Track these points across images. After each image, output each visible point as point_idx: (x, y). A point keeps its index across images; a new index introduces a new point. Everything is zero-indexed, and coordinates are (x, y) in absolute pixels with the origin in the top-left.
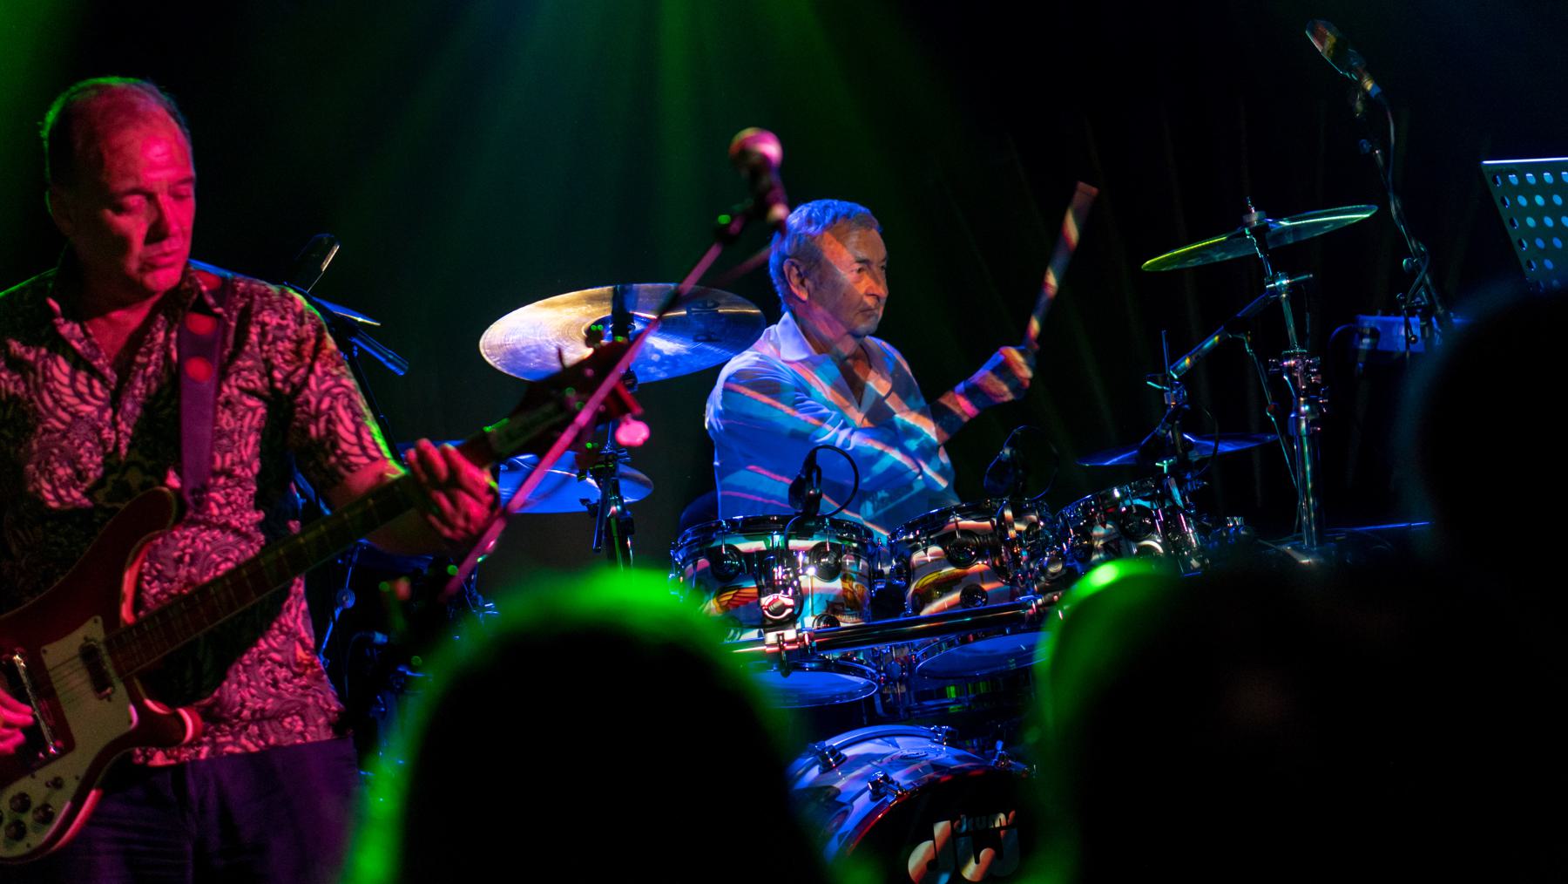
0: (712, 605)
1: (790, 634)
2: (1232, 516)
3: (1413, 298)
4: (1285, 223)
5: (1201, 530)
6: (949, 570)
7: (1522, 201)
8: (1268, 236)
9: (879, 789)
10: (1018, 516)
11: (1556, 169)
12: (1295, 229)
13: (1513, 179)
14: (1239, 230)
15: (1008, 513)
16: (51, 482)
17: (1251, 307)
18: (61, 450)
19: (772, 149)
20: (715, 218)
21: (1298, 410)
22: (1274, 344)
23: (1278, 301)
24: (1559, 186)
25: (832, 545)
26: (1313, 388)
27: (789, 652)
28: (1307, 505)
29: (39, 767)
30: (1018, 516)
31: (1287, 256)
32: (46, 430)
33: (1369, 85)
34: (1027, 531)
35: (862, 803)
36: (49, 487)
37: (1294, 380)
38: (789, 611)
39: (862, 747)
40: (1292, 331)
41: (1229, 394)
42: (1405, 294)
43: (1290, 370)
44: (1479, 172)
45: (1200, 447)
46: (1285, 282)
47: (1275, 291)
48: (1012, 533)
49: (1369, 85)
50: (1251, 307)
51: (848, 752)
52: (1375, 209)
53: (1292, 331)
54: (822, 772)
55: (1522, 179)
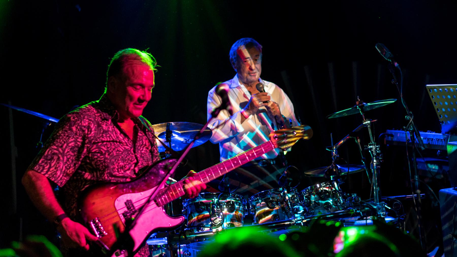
0: (234, 213)
2: (353, 193)
3: (408, 128)
4: (369, 104)
5: (344, 198)
6: (267, 209)
10: (289, 192)
14: (355, 106)
15: (286, 192)
16: (118, 166)
17: (359, 128)
18: (122, 157)
21: (373, 161)
22: (366, 141)
23: (367, 128)
26: (378, 154)
28: (376, 189)
31: (369, 114)
32: (118, 150)
33: (396, 64)
34: (291, 198)
36: (117, 168)
41: (352, 155)
42: (406, 127)
43: (371, 149)
44: (425, 88)
45: (346, 171)
46: (369, 122)
47: (366, 125)
48: (287, 198)
49: (396, 64)
50: (359, 128)
52: (396, 100)
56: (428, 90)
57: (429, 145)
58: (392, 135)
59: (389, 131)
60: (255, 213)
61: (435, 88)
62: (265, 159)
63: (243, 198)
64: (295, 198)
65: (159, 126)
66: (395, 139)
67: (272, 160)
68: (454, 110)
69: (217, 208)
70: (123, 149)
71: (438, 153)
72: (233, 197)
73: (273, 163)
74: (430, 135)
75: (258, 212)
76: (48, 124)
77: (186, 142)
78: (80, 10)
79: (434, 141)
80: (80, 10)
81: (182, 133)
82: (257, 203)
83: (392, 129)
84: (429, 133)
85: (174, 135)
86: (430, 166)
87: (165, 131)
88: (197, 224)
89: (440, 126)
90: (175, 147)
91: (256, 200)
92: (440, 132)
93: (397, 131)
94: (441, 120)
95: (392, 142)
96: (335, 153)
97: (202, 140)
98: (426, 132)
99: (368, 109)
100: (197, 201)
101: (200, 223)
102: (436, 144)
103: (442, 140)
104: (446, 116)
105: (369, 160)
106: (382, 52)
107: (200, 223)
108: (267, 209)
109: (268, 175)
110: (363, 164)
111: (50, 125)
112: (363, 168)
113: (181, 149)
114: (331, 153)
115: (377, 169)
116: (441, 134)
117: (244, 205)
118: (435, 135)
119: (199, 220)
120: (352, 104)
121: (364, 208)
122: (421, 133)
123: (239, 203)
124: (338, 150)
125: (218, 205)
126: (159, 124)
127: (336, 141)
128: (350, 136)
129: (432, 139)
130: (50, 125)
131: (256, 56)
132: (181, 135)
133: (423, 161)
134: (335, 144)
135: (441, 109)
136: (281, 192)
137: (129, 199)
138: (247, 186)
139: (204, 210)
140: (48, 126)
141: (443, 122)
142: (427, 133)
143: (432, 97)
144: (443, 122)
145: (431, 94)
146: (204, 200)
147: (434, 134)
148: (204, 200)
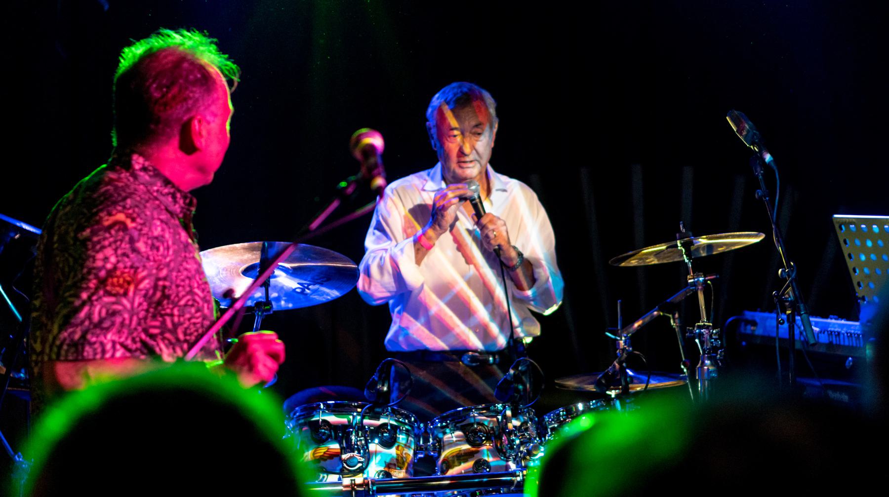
1: (359, 479)
8: (693, 248)
10: (515, 415)
12: (710, 247)
15: (509, 413)
19: (377, 141)
21: (703, 362)
26: (714, 349)
33: (768, 157)
37: (702, 343)
38: (360, 465)
44: (831, 221)
49: (768, 157)
50: (679, 297)
56: (837, 226)
57: (830, 345)
58: (754, 323)
59: (749, 315)
60: (440, 454)
61: (851, 222)
62: (476, 351)
63: (415, 421)
64: (527, 429)
65: (244, 249)
66: (759, 331)
67: (493, 354)
68: (885, 257)
69: (357, 435)
71: (847, 364)
72: (394, 413)
73: (494, 359)
74: (834, 324)
75: (444, 454)
76: (12, 234)
77: (303, 290)
78: (106, 7)
79: (842, 336)
80: (106, 7)
81: (294, 269)
83: (755, 311)
84: (833, 321)
85: (277, 272)
86: (830, 393)
87: (258, 261)
89: (858, 305)
90: (278, 299)
92: (857, 320)
93: (766, 315)
94: (860, 295)
95: (752, 336)
96: (625, 342)
97: (337, 289)
98: (827, 317)
99: (704, 254)
102: (847, 343)
103: (858, 335)
104: (872, 285)
106: (740, 131)
108: (466, 447)
110: (684, 373)
111: (17, 236)
112: (684, 378)
113: (290, 305)
114: (615, 342)
116: (857, 323)
117: (417, 437)
118: (844, 325)
120: (668, 237)
122: (811, 319)
123: (407, 430)
126: (246, 244)
128: (660, 310)
129: (839, 333)
130: (17, 236)
131: (476, 126)
132: (294, 273)
133: (818, 383)
135: (862, 271)
136: (498, 412)
140: (13, 238)
141: (863, 298)
142: (829, 321)
143: (845, 241)
144: (863, 298)
145: (842, 234)
146: (332, 419)
147: (843, 322)
148: (332, 419)
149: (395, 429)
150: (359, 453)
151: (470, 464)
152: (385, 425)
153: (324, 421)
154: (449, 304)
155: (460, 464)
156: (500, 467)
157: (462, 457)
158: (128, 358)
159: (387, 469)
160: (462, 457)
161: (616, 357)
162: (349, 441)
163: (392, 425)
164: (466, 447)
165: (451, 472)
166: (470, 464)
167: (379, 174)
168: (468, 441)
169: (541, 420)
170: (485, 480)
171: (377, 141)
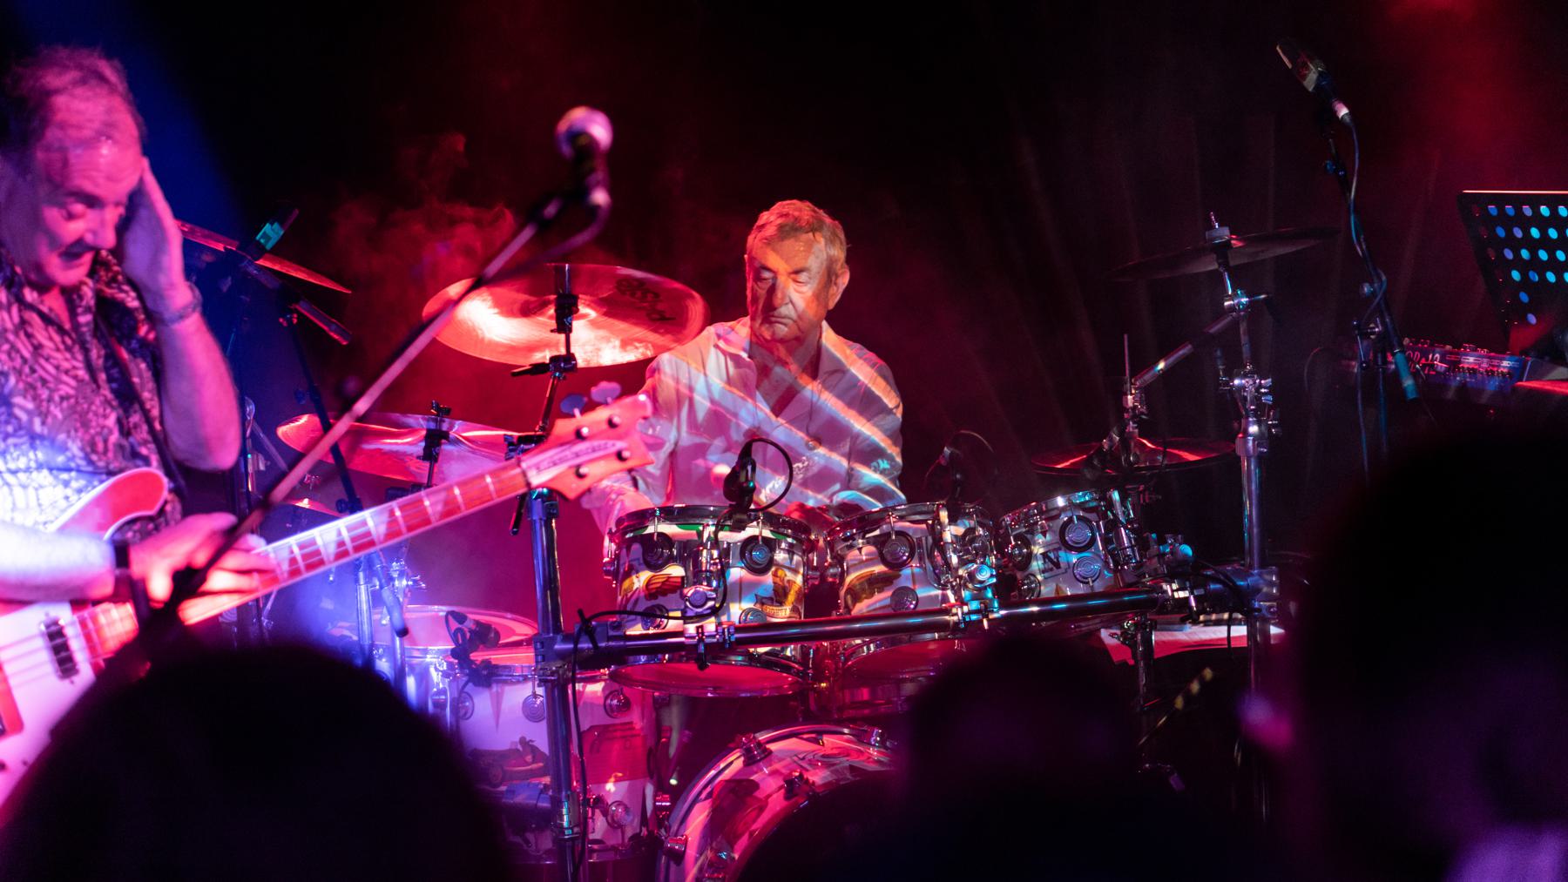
1: (710, 625)
7: (1501, 232)
9: (792, 786)
10: (953, 520)
11: (1553, 202)
13: (1493, 209)
19: (600, 130)
20: (1341, 122)
24: (1555, 220)
25: (1079, 518)
27: (706, 645)
29: (512, 683)
30: (953, 520)
31: (301, 315)
35: (777, 803)
38: (710, 603)
39: (786, 747)
40: (1246, 349)
48: (948, 537)
51: (773, 747)
53: (1246, 349)
54: (746, 764)
55: (1519, 210)
70: (73, 383)
75: (848, 580)
82: (851, 547)
88: (643, 605)
91: (846, 539)
100: (650, 530)
101: (654, 602)
105: (1231, 427)
107: (654, 602)
108: (879, 568)
109: (893, 481)
115: (1261, 459)
119: (652, 592)
121: (1205, 586)
123: (791, 545)
124: (1147, 393)
125: (713, 547)
127: (1142, 364)
134: (1135, 373)
137: (76, 679)
138: (811, 503)
139: (671, 560)
149: (770, 545)
150: (709, 585)
151: (887, 594)
152: (753, 539)
153: (661, 534)
154: (840, 370)
155: (872, 595)
156: (933, 599)
157: (876, 583)
158: (244, 432)
159: (758, 607)
160: (876, 583)
161: (157, 621)
162: (697, 564)
163: (765, 539)
164: (879, 568)
165: (861, 608)
166: (887, 594)
167: (597, 184)
168: (884, 561)
169: (998, 526)
170: (762, 650)
171: (600, 130)
